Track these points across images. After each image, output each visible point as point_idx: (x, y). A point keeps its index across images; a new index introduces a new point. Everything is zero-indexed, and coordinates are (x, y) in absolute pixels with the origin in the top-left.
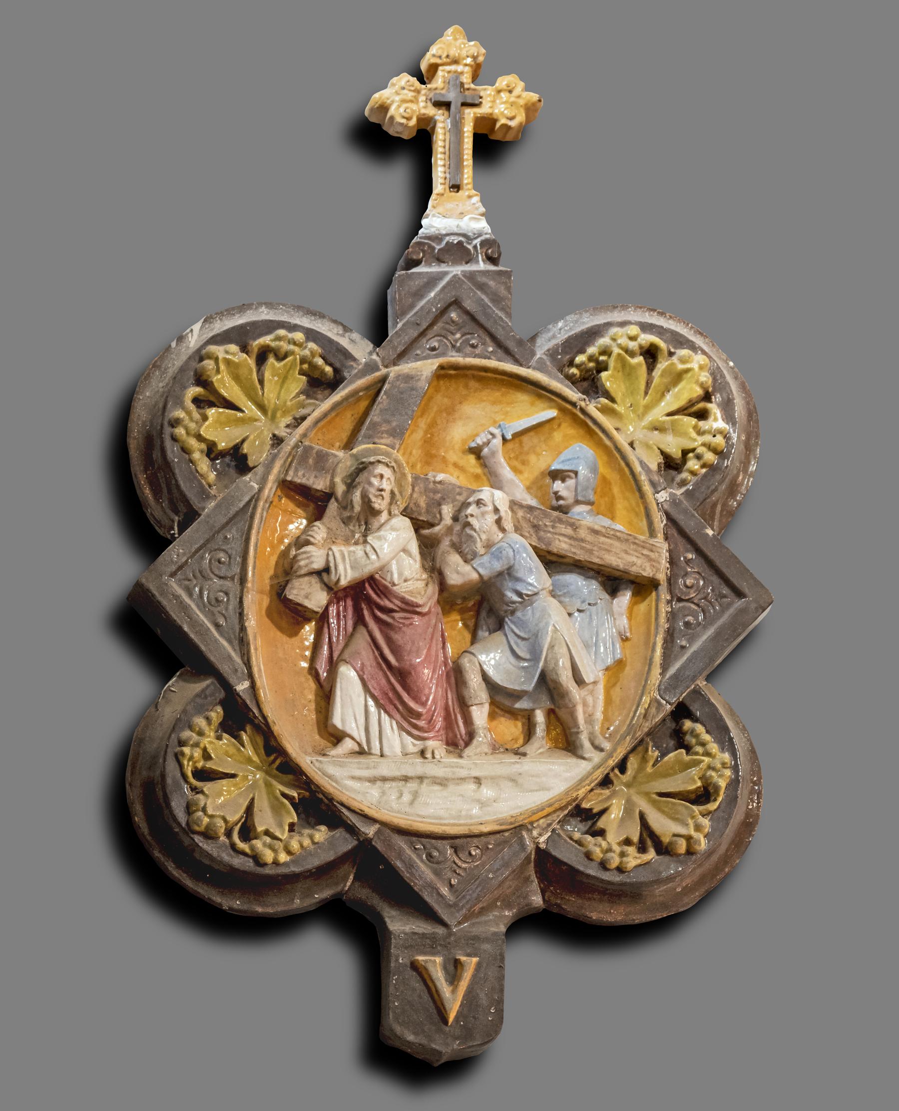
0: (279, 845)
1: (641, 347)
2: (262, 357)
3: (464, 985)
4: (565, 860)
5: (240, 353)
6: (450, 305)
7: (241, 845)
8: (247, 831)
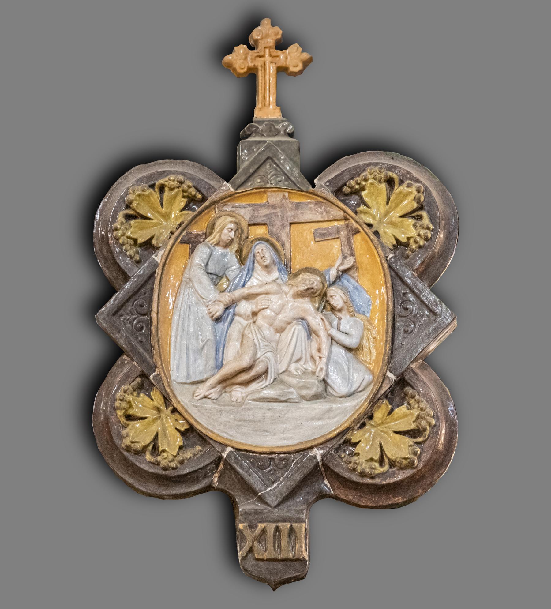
2: (162, 189)
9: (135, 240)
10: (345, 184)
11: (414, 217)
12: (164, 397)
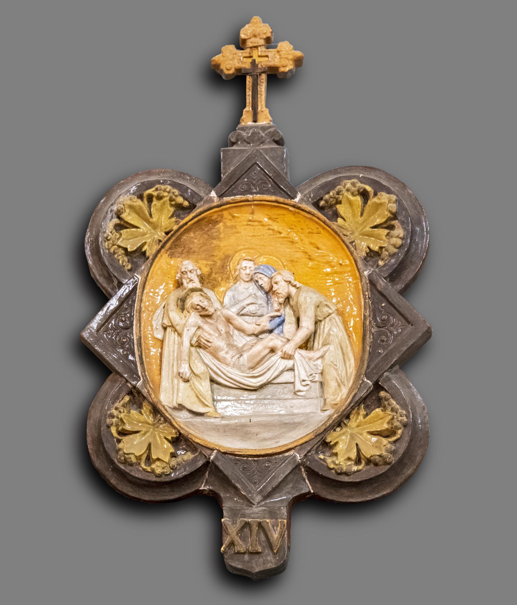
1: (358, 191)
2: (150, 199)
6: (254, 164)
8: (149, 460)
9: (126, 249)
10: (321, 199)
11: (386, 228)
12: (214, 429)
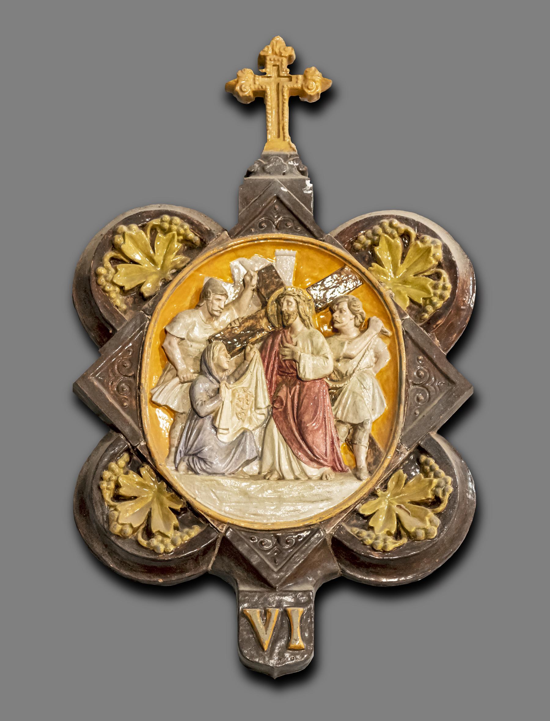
0: (168, 541)
3: (272, 625)
4: (144, 365)
5: (343, 487)
7: (144, 543)
8: (149, 533)
